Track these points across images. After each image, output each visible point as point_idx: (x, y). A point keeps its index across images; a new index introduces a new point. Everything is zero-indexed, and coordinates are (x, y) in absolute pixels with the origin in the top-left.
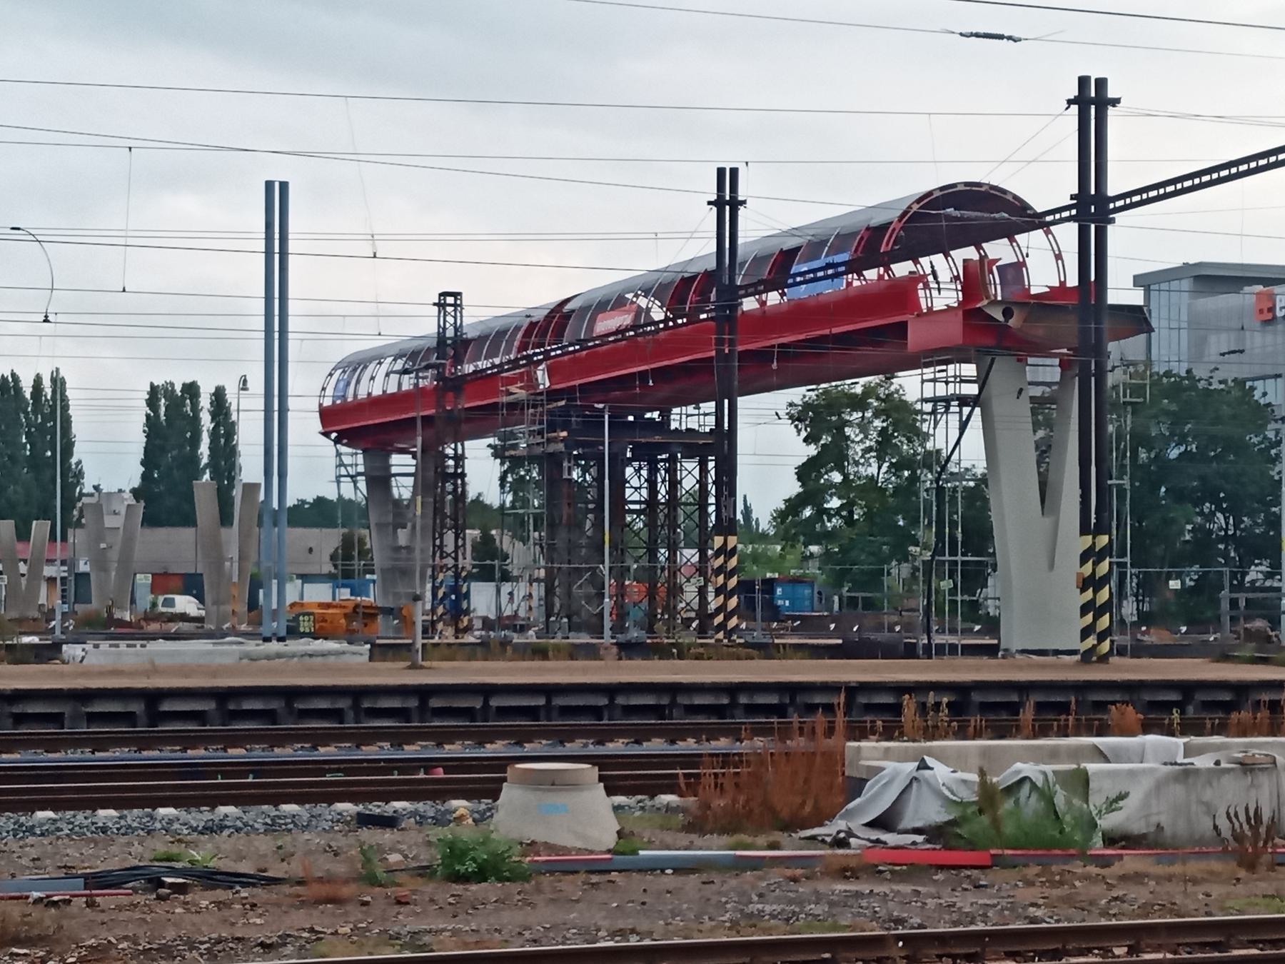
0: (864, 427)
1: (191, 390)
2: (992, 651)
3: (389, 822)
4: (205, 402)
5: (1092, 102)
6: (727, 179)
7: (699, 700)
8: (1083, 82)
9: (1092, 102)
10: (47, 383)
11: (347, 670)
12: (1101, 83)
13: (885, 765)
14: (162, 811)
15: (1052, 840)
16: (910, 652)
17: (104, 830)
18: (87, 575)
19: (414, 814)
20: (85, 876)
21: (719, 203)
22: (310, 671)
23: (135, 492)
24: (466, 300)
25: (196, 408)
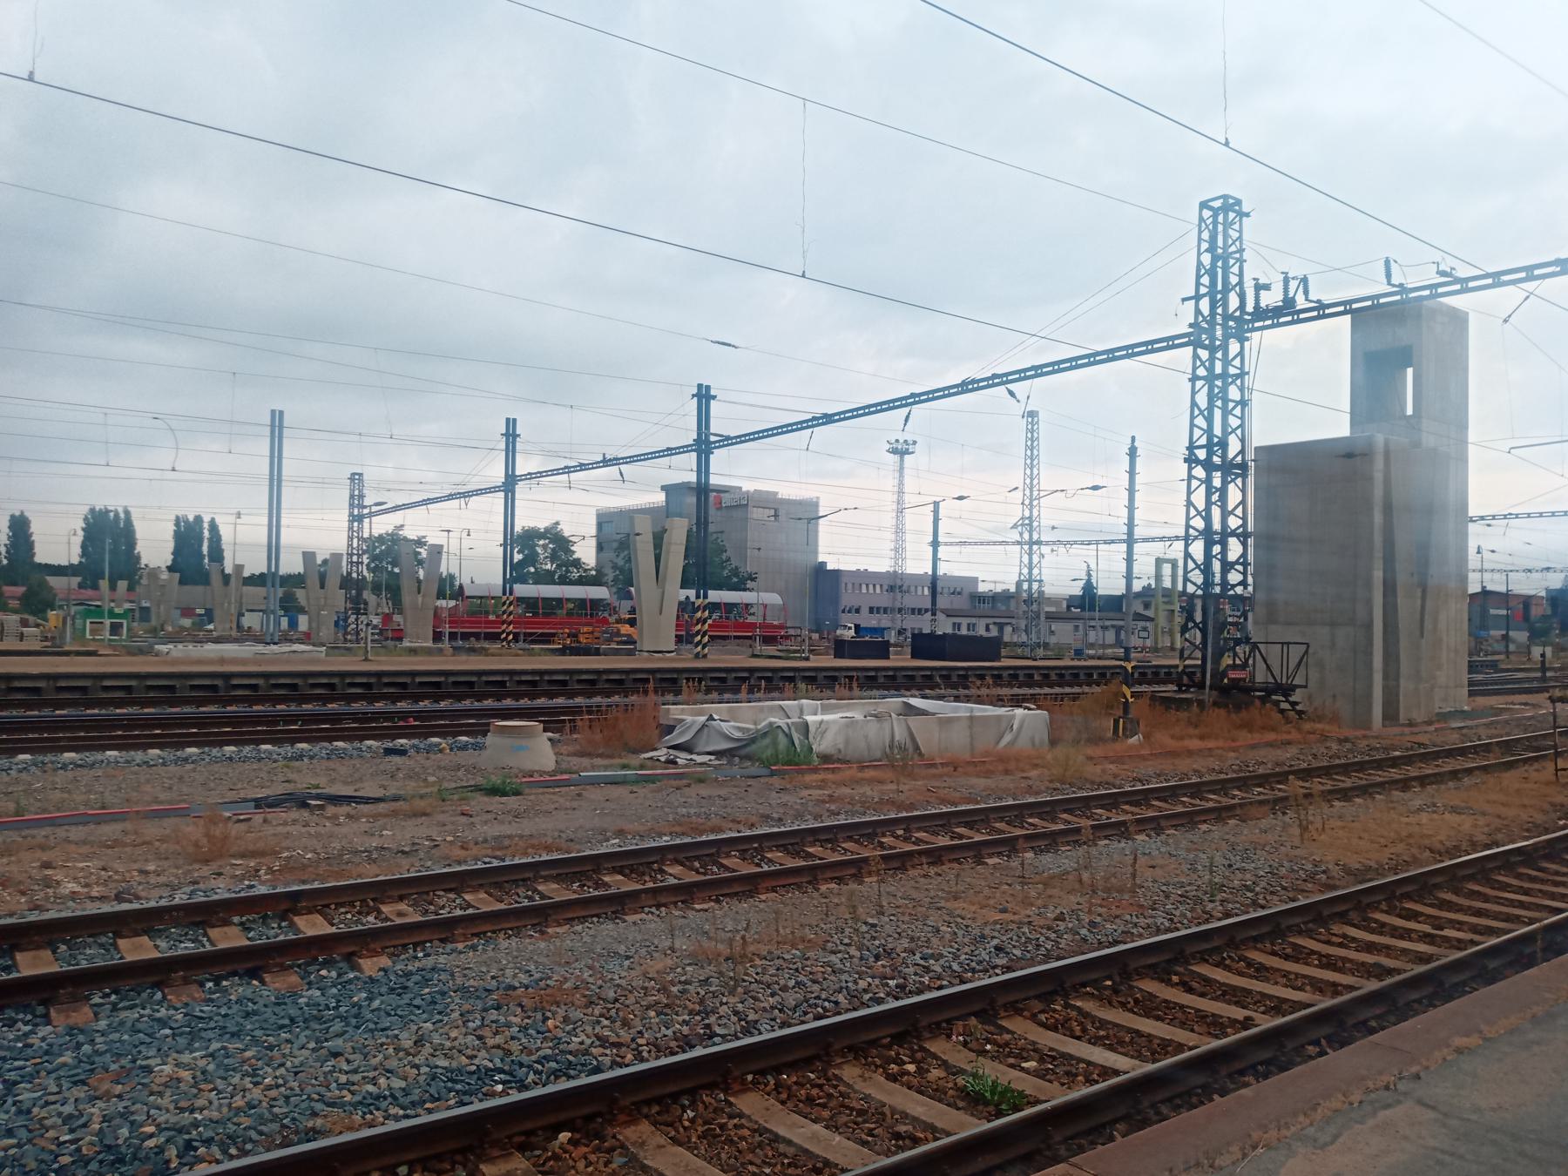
0: (545, 547)
1: (198, 519)
2: (630, 653)
3: (401, 752)
4: (206, 525)
5: (704, 396)
6: (511, 424)
7: (524, 678)
8: (700, 386)
9: (704, 396)
10: (122, 516)
11: (318, 661)
12: (708, 388)
13: (687, 715)
14: (264, 747)
15: (789, 759)
16: (597, 652)
17: (231, 759)
18: (147, 609)
19: (414, 746)
20: (256, 800)
21: (515, 436)
22: (288, 662)
23: (170, 569)
24: (365, 477)
25: (201, 529)
